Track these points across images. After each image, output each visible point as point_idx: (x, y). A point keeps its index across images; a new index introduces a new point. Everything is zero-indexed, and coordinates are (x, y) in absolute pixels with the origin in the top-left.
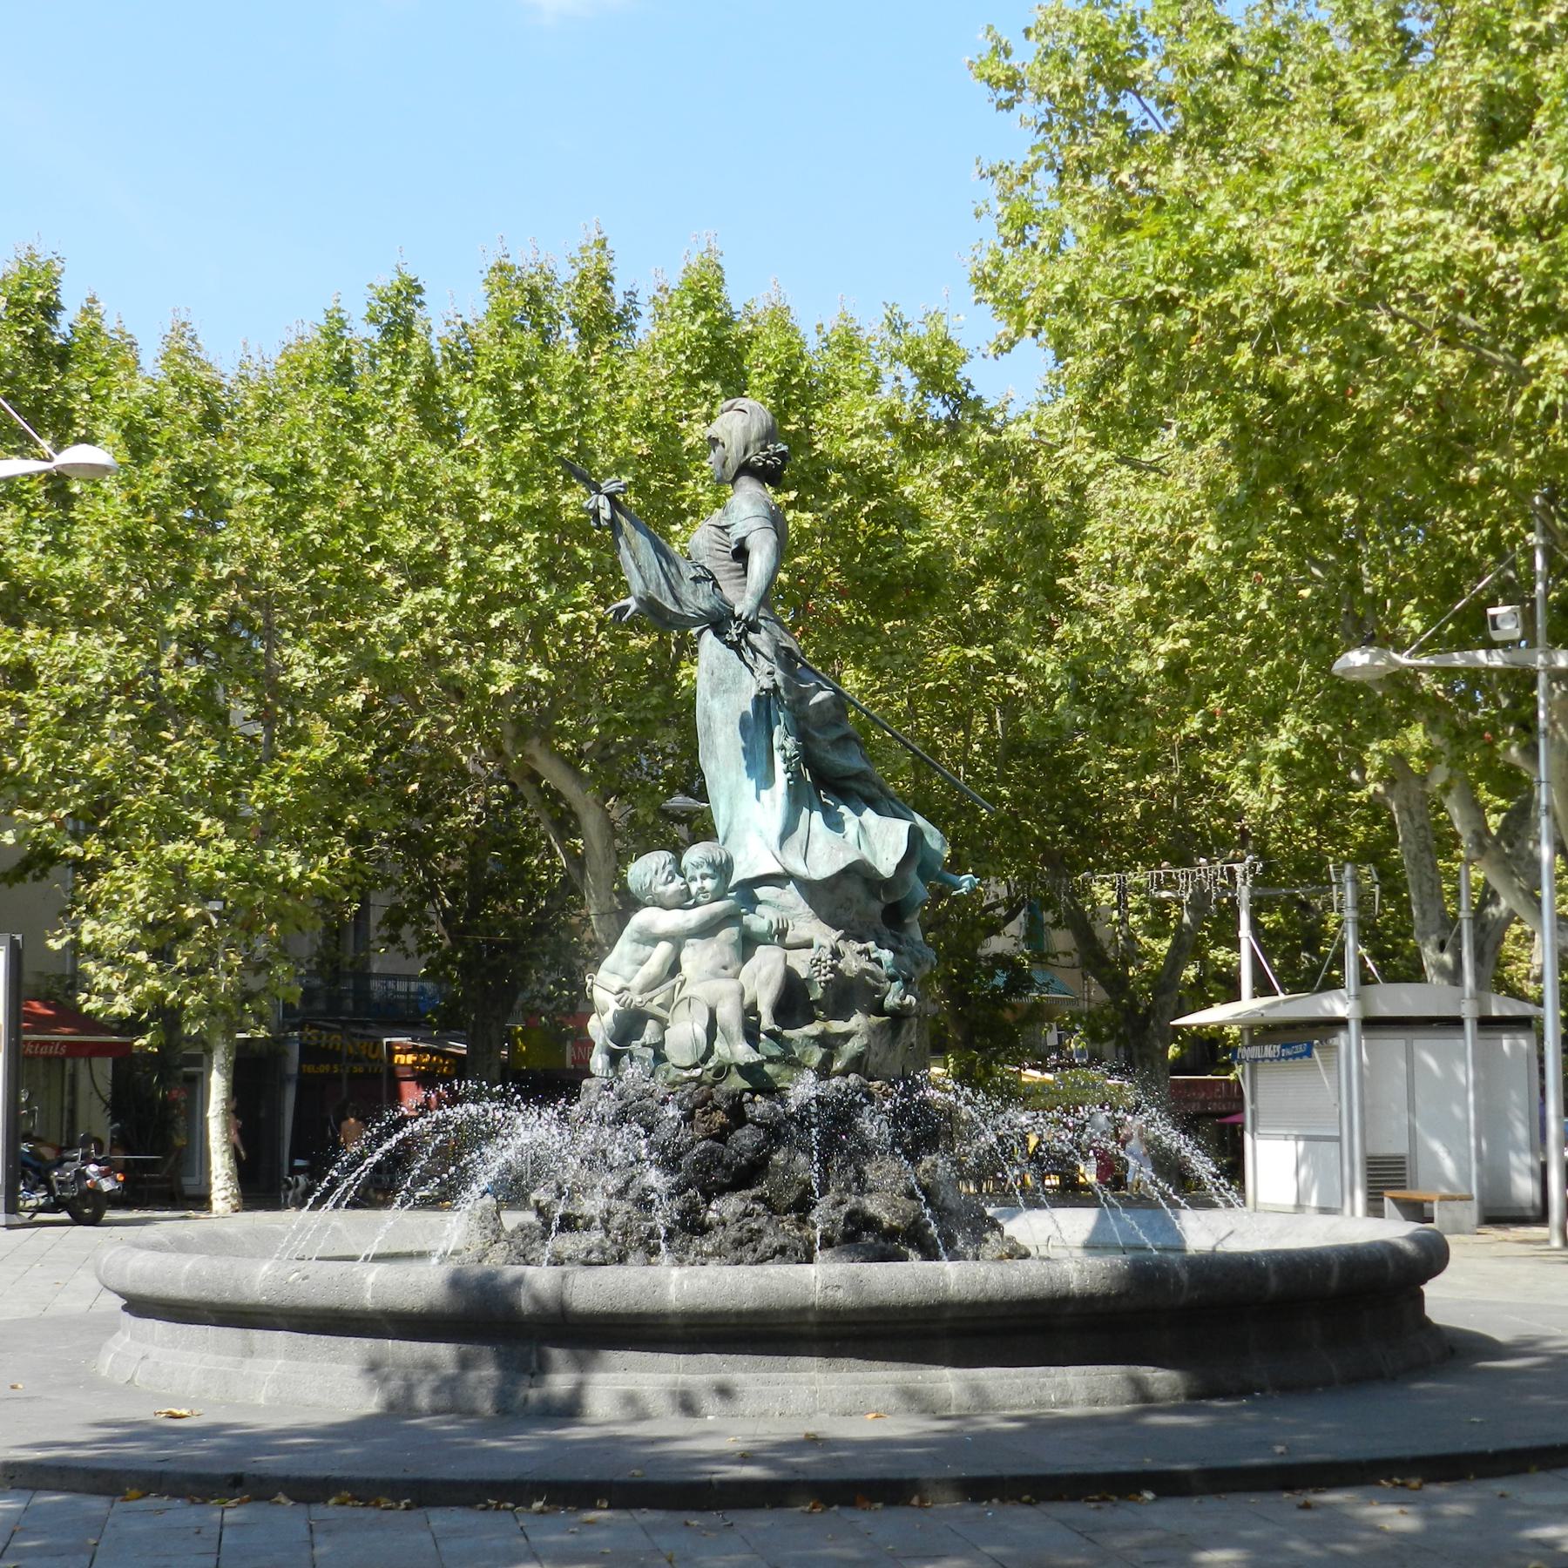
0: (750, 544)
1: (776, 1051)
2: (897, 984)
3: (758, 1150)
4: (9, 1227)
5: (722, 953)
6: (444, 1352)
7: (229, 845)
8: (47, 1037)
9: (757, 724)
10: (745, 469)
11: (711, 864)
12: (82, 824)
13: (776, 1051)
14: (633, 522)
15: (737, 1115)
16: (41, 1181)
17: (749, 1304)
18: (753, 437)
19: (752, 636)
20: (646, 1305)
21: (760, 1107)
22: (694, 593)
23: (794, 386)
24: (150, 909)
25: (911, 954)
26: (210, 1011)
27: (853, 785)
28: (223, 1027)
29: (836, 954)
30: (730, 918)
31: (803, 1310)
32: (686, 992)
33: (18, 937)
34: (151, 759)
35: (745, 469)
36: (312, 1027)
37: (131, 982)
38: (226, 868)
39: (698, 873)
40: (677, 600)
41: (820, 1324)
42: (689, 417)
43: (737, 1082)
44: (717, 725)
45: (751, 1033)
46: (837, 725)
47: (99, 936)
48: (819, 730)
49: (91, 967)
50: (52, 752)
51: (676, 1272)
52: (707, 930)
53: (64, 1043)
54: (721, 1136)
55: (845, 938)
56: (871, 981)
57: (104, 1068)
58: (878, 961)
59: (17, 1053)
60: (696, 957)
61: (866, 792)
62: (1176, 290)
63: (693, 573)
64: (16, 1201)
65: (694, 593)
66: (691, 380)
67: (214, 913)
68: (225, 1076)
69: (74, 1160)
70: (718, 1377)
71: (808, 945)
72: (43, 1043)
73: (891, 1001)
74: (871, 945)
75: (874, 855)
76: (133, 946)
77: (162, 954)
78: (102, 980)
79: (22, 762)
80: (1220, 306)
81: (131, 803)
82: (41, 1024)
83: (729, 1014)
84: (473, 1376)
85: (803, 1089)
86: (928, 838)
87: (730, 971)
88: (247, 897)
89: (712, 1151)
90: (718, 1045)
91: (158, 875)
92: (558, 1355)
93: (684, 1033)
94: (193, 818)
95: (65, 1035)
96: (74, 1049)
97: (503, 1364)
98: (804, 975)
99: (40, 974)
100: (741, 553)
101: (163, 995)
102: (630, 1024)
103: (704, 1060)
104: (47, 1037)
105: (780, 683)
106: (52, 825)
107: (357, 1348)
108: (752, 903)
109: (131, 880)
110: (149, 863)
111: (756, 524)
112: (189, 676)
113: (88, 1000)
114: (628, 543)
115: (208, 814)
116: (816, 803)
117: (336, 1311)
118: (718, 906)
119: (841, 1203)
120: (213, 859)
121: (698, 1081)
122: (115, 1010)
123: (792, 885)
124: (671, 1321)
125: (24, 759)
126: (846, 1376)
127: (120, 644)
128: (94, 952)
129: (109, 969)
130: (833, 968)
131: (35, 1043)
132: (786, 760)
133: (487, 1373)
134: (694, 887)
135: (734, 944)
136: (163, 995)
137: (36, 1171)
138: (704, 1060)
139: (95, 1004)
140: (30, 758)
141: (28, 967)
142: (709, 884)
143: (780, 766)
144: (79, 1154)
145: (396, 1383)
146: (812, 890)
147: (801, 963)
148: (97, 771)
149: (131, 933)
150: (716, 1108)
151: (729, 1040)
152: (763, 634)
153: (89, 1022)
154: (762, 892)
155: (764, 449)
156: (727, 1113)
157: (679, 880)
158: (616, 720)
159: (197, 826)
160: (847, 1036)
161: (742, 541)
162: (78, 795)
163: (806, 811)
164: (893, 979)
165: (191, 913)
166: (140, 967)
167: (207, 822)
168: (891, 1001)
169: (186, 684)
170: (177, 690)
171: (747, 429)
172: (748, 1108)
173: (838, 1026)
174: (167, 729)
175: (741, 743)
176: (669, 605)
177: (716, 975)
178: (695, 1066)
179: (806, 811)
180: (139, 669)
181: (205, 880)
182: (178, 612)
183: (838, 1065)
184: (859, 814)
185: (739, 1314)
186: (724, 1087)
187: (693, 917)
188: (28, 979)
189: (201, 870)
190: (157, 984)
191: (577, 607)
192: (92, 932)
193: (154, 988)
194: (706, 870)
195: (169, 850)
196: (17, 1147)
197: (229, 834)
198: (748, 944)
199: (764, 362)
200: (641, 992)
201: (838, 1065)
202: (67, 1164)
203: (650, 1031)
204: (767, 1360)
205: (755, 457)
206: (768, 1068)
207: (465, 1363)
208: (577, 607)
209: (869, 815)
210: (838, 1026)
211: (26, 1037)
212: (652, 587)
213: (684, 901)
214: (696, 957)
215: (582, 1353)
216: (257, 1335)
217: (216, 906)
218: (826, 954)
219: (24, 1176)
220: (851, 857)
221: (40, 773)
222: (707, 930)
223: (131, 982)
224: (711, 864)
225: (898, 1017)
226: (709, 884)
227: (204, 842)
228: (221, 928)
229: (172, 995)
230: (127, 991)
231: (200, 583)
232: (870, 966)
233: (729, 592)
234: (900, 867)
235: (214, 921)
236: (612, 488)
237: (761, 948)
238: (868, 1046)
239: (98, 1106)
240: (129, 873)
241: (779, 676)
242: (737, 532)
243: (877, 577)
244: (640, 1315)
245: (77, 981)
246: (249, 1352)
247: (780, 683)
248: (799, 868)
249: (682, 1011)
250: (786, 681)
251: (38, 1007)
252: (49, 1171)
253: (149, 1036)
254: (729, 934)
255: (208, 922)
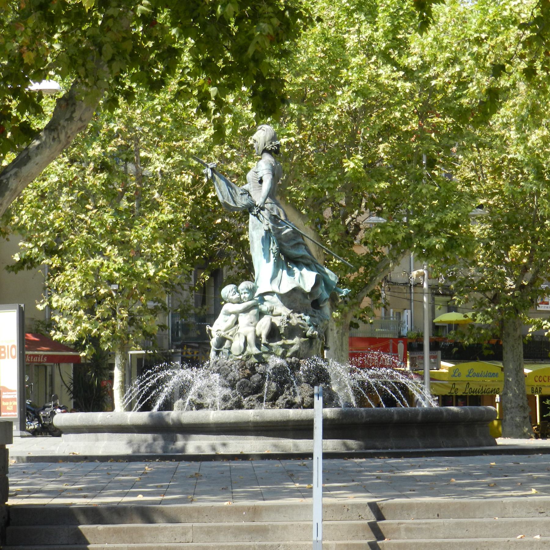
0: (264, 179)
1: (266, 350)
2: (311, 328)
3: (259, 382)
4: (22, 436)
5: (251, 318)
6: (149, 437)
7: (120, 260)
8: (36, 353)
9: (266, 239)
10: (265, 151)
11: (247, 289)
12: (50, 251)
13: (266, 350)
14: (219, 177)
15: (253, 369)
16: (35, 417)
17: (232, 421)
18: (267, 139)
19: (262, 212)
20: (204, 421)
21: (260, 368)
22: (241, 199)
23: (401, 15)
24: (83, 290)
25: (319, 317)
26: (112, 338)
27: (300, 260)
28: (119, 346)
29: (289, 318)
30: (255, 306)
31: (248, 422)
32: (239, 331)
33: (22, 305)
34: (82, 216)
35: (265, 151)
36: (188, 347)
37: (76, 324)
38: (119, 270)
39: (243, 292)
40: (235, 202)
41: (254, 427)
42: (348, 32)
43: (253, 360)
44: (255, 240)
45: (258, 344)
46: (294, 240)
47: (60, 304)
48: (286, 242)
49: (57, 318)
50: (35, 215)
51: (213, 412)
52: (246, 311)
53: (45, 356)
54: (248, 377)
55: (293, 312)
56: (302, 327)
57: (68, 370)
58: (305, 320)
59: (23, 361)
60: (244, 319)
61: (305, 262)
62: (483, 36)
63: (241, 192)
64: (25, 426)
65: (241, 199)
66: (350, 13)
67: (114, 290)
68: (121, 370)
69: (50, 407)
70: (222, 442)
71: (280, 315)
72: (34, 356)
73: (309, 333)
74: (302, 315)
75: (304, 284)
76: (76, 308)
77: (91, 311)
78: (62, 325)
79: (21, 219)
80: (501, 42)
81: (72, 239)
82: (33, 345)
83: (251, 339)
84: (156, 443)
85: (275, 361)
86: (330, 277)
87: (253, 324)
88: (128, 284)
89: (245, 382)
90: (248, 349)
91: (86, 274)
92: (179, 436)
93: (237, 344)
94: (102, 245)
95: (44, 351)
96: (50, 359)
97: (165, 439)
98: (278, 325)
99: (32, 319)
100: (261, 181)
101: (90, 331)
102: (222, 341)
103: (243, 353)
104: (36, 353)
105: (271, 228)
106: (37, 250)
107: (126, 436)
108: (262, 301)
109: (74, 276)
110: (82, 268)
111: (265, 172)
112: (99, 178)
113: (55, 334)
114: (218, 184)
115: (110, 244)
116: (285, 267)
117: (120, 425)
118: (250, 303)
119: (286, 398)
120: (112, 266)
121: (241, 360)
122: (68, 339)
123: (275, 295)
124: (212, 426)
125: (22, 219)
126: (262, 441)
127: (66, 163)
128: (60, 311)
129: (65, 319)
130: (287, 323)
131: (30, 356)
132: (274, 253)
133: (160, 443)
134: (242, 296)
135: (255, 315)
136: (90, 331)
137: (33, 412)
138: (243, 353)
139: (58, 336)
140: (25, 217)
141: (27, 315)
142: (247, 295)
143: (272, 255)
144: (52, 404)
145: (136, 446)
146: (284, 298)
147: (277, 321)
148: (57, 225)
149: (75, 301)
150: (246, 368)
151: (251, 347)
152: (266, 211)
153: (58, 345)
154: (266, 297)
155: (271, 143)
156: (250, 370)
157: (237, 294)
158: (313, 189)
159: (105, 250)
160: (292, 345)
161: (261, 178)
162: (48, 236)
163: (281, 270)
164: (310, 326)
165: (102, 291)
166: (80, 318)
167: (110, 248)
168: (309, 333)
169: (98, 182)
170: (94, 185)
171: (265, 137)
172: (256, 368)
173: (289, 342)
174: (89, 204)
175: (262, 247)
176: (232, 204)
177: (248, 325)
178: (240, 355)
179: (281, 270)
180: (75, 175)
181: (108, 276)
182: (93, 149)
183: (289, 354)
184: (301, 269)
185: (230, 423)
186: (249, 362)
187: (241, 307)
188: (27, 322)
189: (106, 271)
190: (88, 325)
191: (289, 135)
192: (57, 301)
193: (86, 328)
194: (246, 291)
195: (91, 262)
196: (24, 401)
197: (120, 254)
198: (261, 314)
199: (386, 4)
200: (225, 331)
201: (289, 354)
202: (46, 409)
203: (227, 343)
204: (239, 437)
205: (269, 147)
206: (264, 356)
207: (155, 440)
208: (289, 135)
209: (305, 271)
210: (289, 342)
211: (27, 353)
212: (226, 198)
213: (240, 301)
214: (244, 319)
215: (187, 436)
216: (99, 435)
217: (115, 287)
218: (285, 318)
219: (28, 414)
220: (294, 286)
221: (30, 224)
222: (246, 311)
223: (76, 324)
224: (247, 289)
225: (312, 338)
226: (247, 295)
227: (108, 258)
228: (118, 298)
229: (95, 331)
230: (73, 329)
231: (104, 134)
232: (301, 322)
233: (254, 198)
234: (313, 288)
235: (114, 294)
236: (212, 166)
237: (265, 316)
238: (300, 348)
239: (65, 389)
240: (73, 273)
241: (271, 225)
242: (260, 175)
243: (454, 108)
244: (203, 424)
245: (51, 325)
246: (97, 440)
247: (271, 228)
248: (277, 290)
249: (237, 337)
250: (273, 227)
251: (30, 337)
252: (38, 413)
253: (86, 351)
254: (254, 312)
255: (111, 295)
